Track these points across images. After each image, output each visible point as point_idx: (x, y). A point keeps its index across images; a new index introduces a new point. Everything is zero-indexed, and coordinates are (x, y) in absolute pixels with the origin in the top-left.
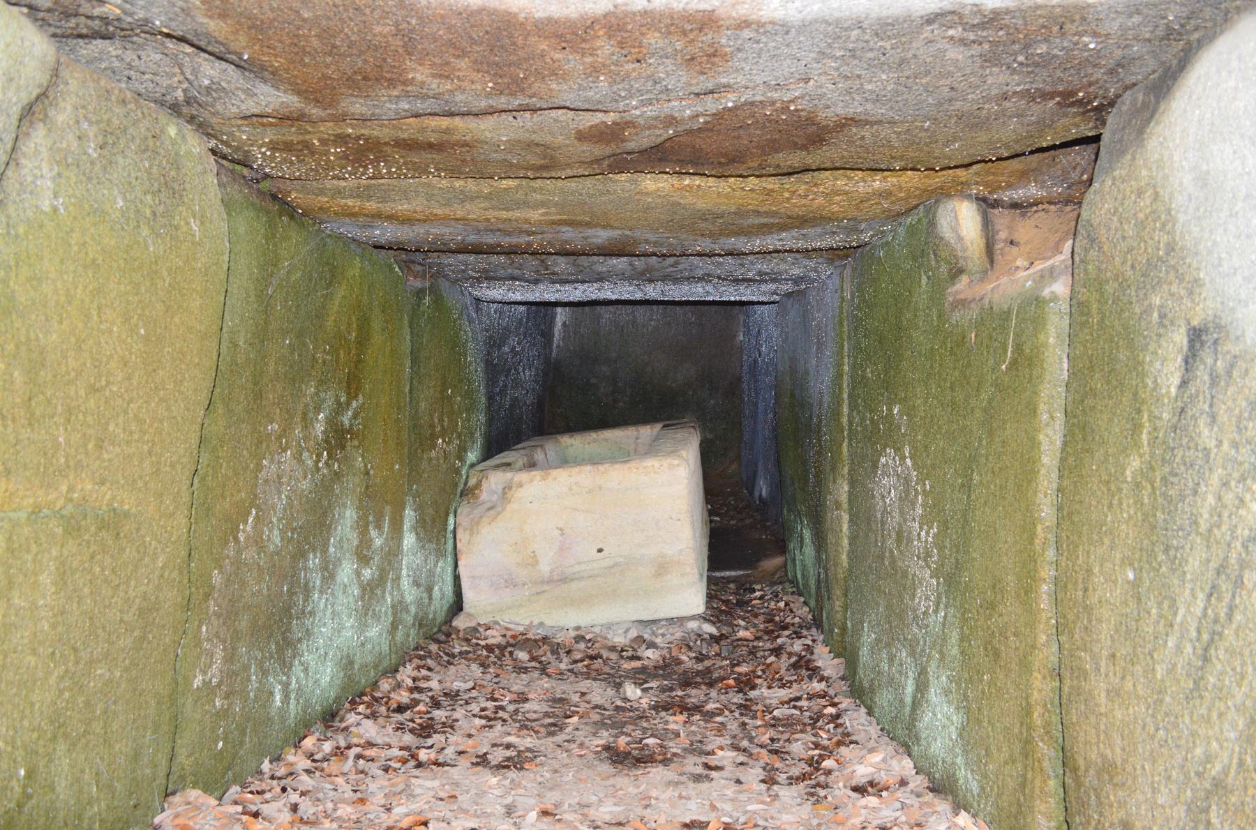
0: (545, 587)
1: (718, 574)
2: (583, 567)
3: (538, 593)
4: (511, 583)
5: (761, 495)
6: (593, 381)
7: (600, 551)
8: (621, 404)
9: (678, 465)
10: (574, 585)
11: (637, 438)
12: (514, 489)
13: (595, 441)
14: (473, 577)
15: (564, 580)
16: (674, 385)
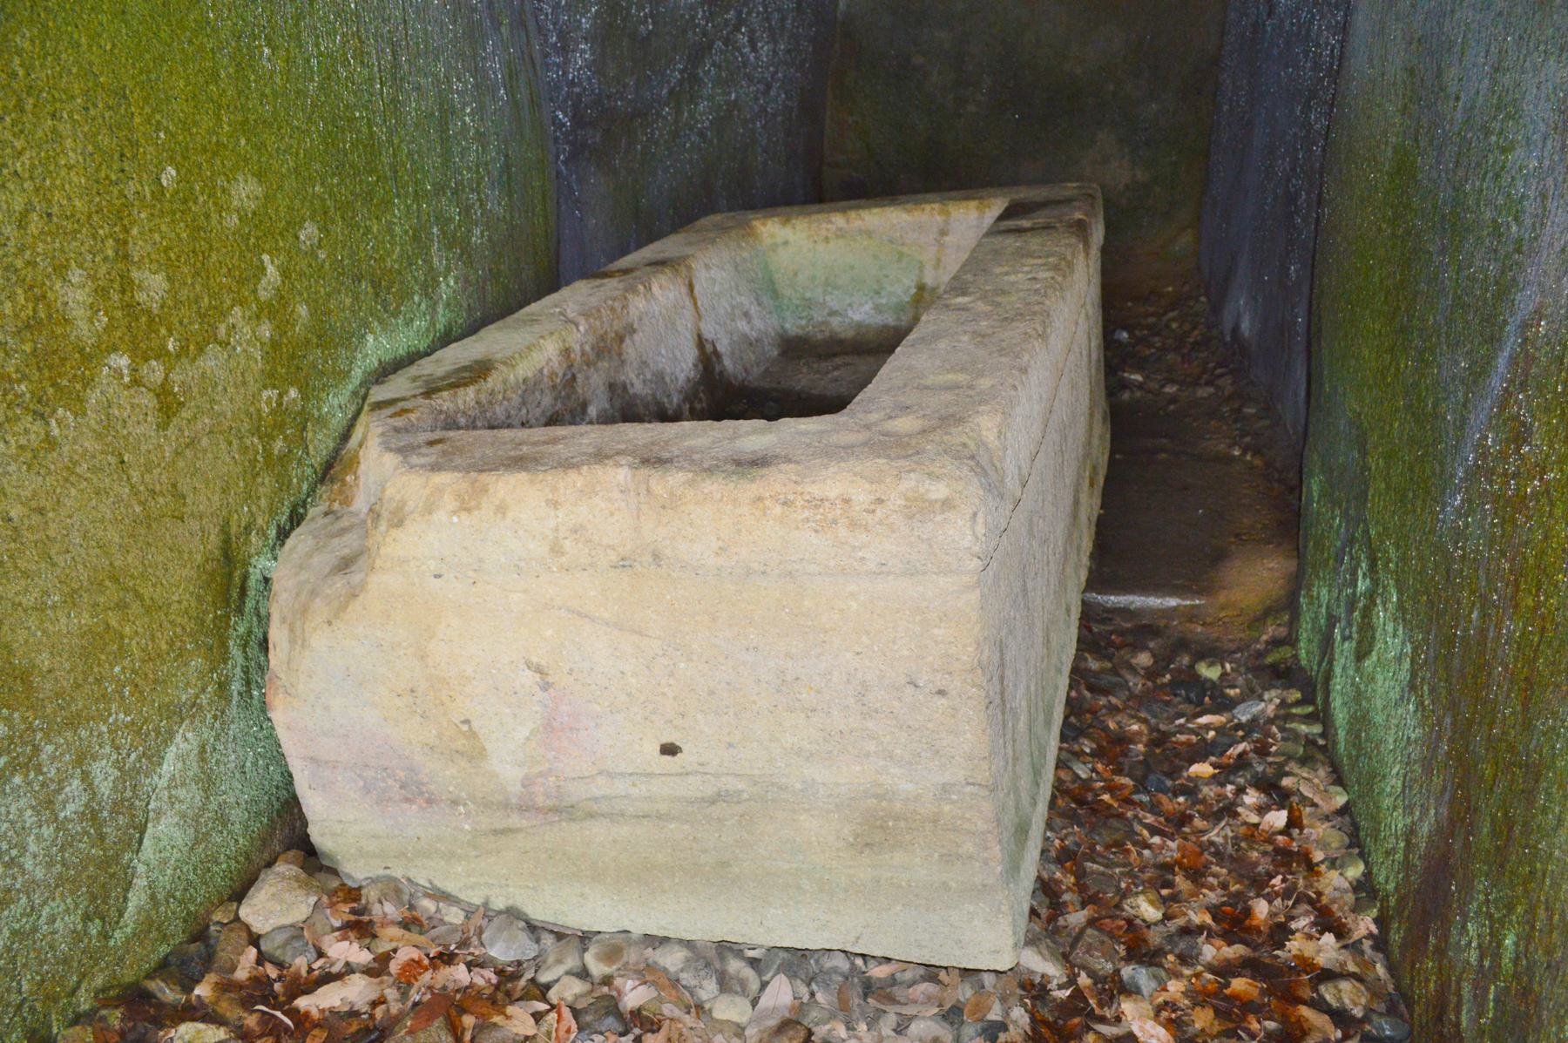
0: (515, 820)
1: (1114, 600)
2: (621, 787)
3: (495, 832)
4: (415, 792)
5: (1236, 330)
6: (918, 60)
7: (670, 750)
8: (971, 108)
9: (947, 504)
10: (598, 831)
11: (943, 233)
12: (383, 526)
13: (841, 234)
14: (313, 760)
15: (564, 811)
16: (1079, 71)
